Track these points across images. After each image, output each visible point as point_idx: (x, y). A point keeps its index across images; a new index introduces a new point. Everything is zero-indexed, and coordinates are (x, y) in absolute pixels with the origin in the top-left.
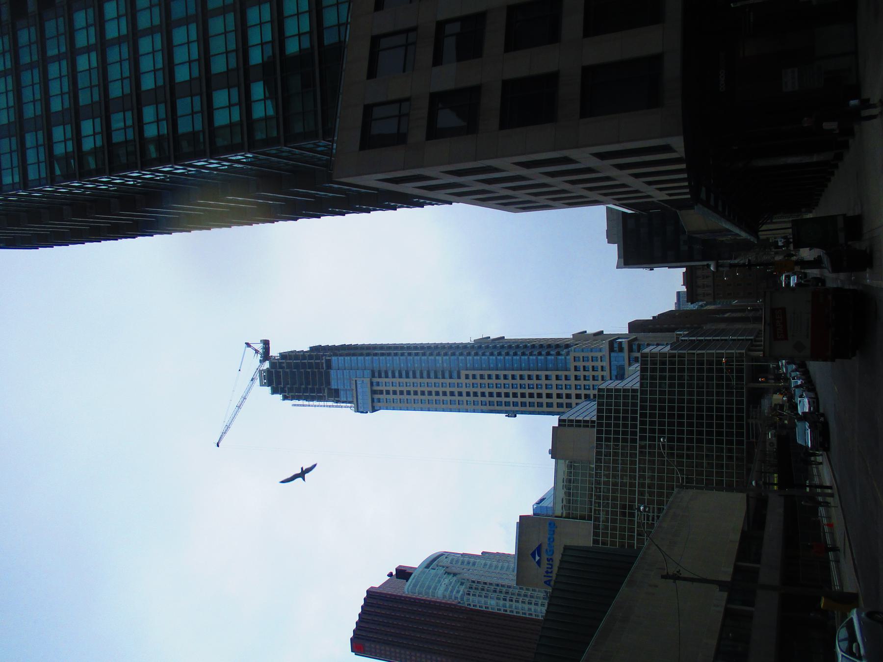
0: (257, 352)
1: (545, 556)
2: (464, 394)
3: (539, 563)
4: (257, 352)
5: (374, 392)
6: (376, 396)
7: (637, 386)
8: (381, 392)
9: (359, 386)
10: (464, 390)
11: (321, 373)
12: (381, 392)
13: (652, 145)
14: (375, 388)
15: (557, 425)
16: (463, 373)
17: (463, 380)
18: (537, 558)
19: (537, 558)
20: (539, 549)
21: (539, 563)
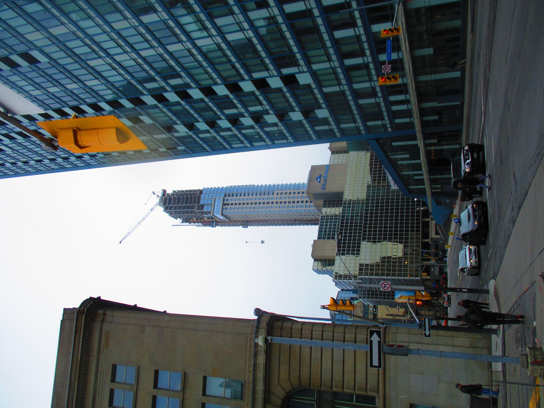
0: (158, 196)
1: (323, 179)
2: (275, 203)
3: (319, 182)
4: (158, 196)
5: (224, 204)
6: (225, 207)
7: (362, 243)
8: (228, 204)
9: (216, 201)
10: (275, 201)
11: (195, 197)
12: (228, 204)
13: (449, 77)
14: (225, 202)
15: (316, 239)
16: (275, 193)
17: (275, 196)
18: (319, 180)
19: (319, 180)
20: (320, 177)
21: (319, 182)
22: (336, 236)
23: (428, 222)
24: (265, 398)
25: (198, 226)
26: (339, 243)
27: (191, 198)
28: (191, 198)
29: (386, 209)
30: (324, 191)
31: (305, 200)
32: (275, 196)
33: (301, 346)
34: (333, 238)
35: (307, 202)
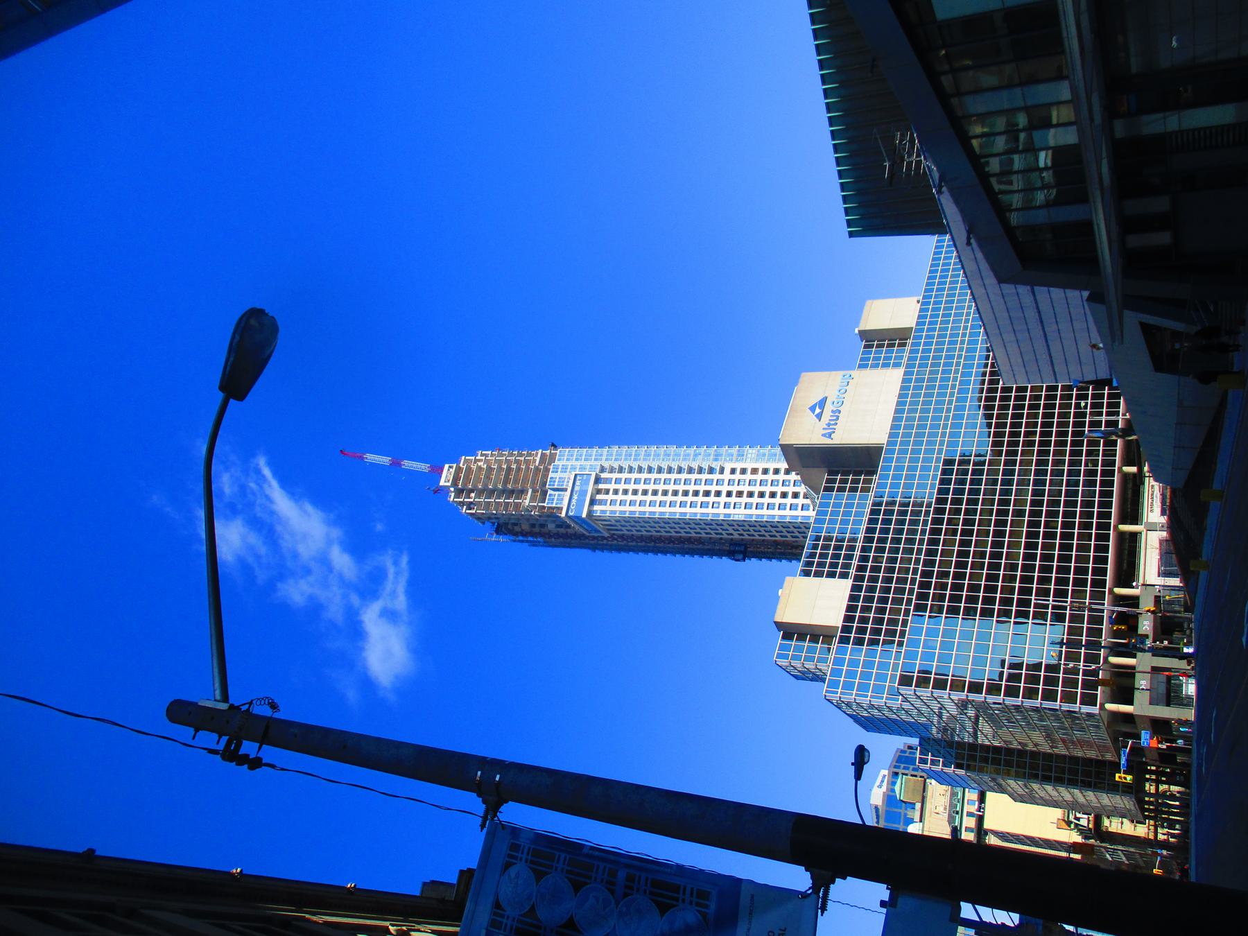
2: (724, 494)
9: (578, 483)
13: (687, 861)
17: (727, 476)
18: (818, 411)
19: (818, 411)
20: (822, 403)
21: (819, 416)
22: (852, 571)
23: (1134, 536)
24: (988, 316)
25: (534, 544)
26: (856, 588)
27: (519, 469)
28: (519, 469)
29: (892, 570)
30: (827, 441)
31: (790, 490)
32: (727, 476)
33: (753, 896)
34: (844, 576)
35: (776, 471)
